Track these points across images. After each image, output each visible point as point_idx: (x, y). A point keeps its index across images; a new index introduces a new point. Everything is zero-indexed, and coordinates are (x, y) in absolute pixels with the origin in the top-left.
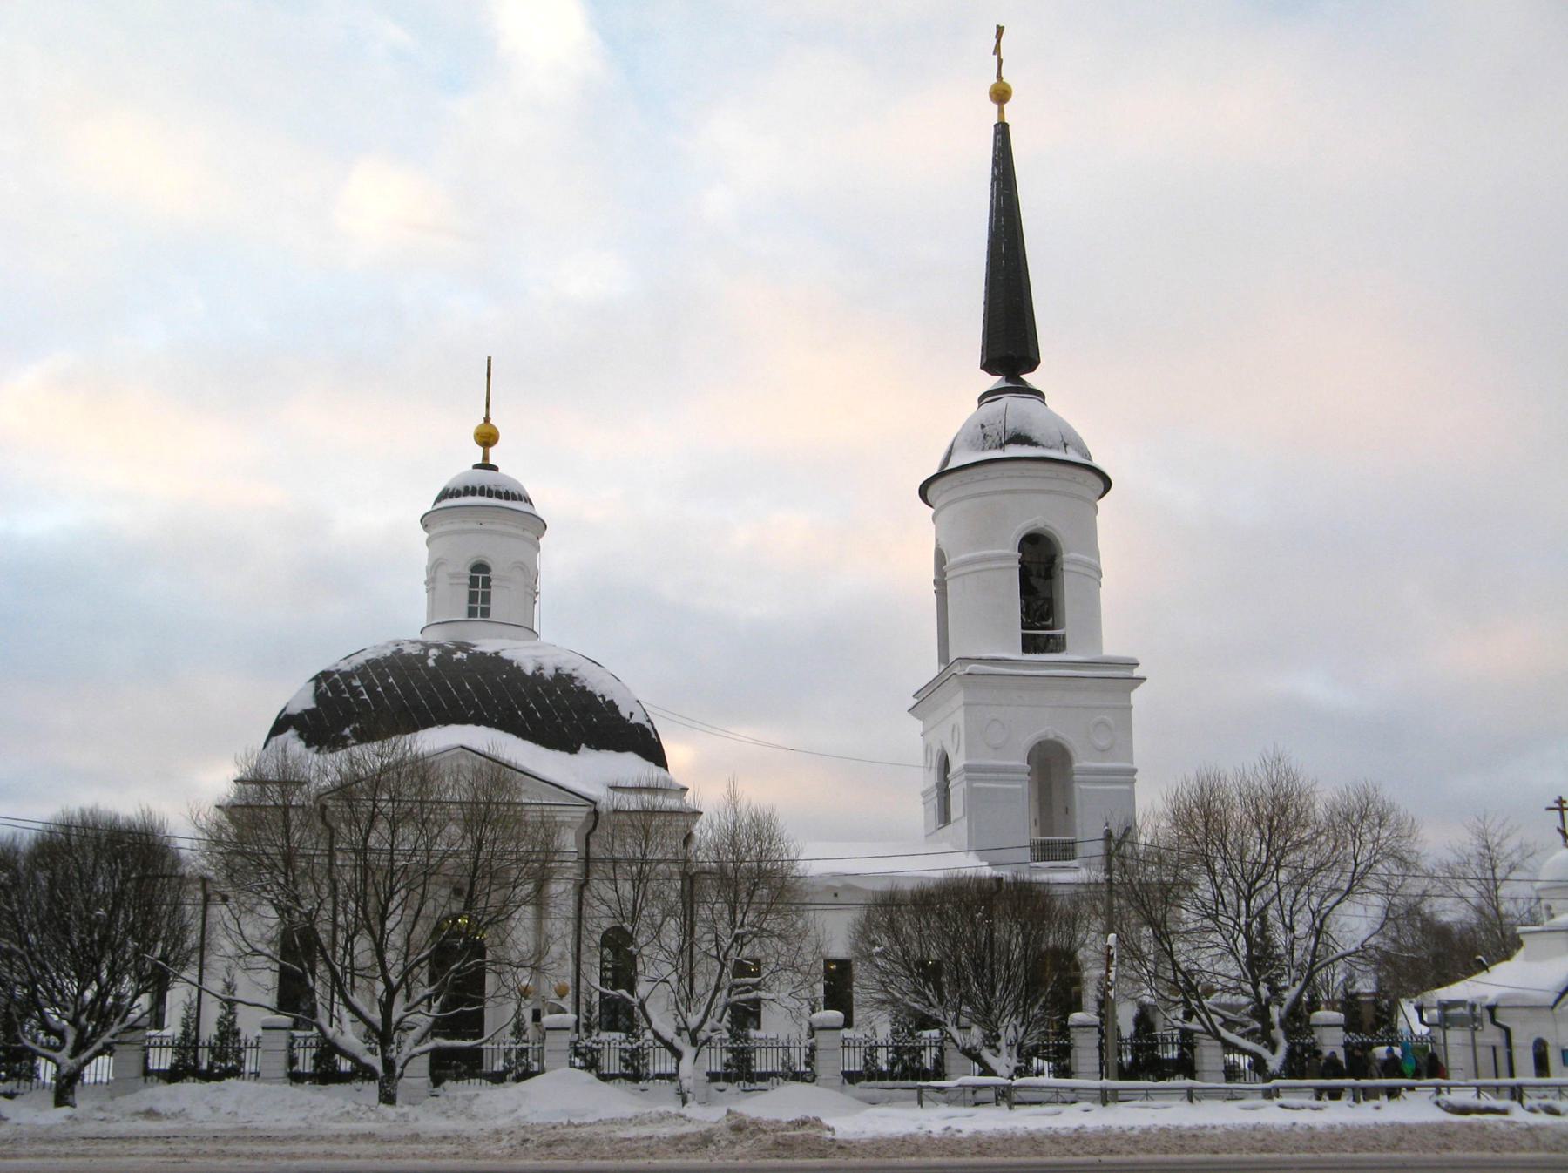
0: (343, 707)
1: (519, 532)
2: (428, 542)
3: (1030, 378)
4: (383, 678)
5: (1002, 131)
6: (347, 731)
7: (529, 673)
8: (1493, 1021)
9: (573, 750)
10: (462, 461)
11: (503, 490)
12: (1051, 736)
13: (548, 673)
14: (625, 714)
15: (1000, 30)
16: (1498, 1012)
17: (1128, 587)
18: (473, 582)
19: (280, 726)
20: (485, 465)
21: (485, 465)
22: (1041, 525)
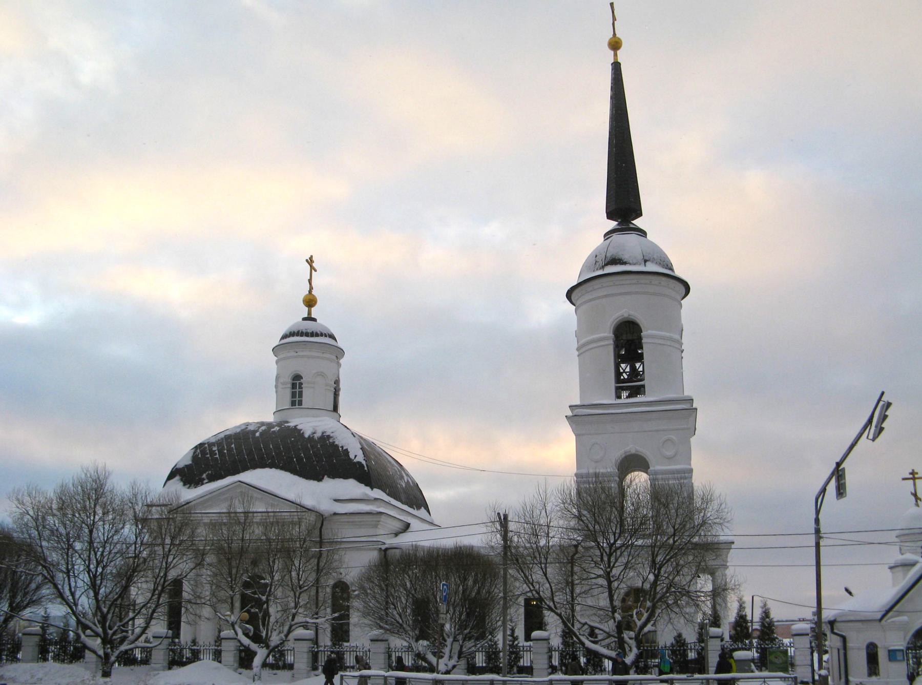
0: (212, 462)
1: (320, 355)
2: (277, 362)
3: (638, 222)
4: (229, 444)
5: (616, 68)
6: (204, 476)
7: (306, 436)
8: (832, 632)
9: (319, 479)
10: (295, 316)
11: (324, 332)
12: (633, 451)
13: (318, 435)
14: (352, 456)
15: (612, 4)
16: (837, 625)
17: (698, 352)
18: (294, 386)
19: (171, 476)
20: (309, 318)
21: (309, 318)
22: (626, 315)
